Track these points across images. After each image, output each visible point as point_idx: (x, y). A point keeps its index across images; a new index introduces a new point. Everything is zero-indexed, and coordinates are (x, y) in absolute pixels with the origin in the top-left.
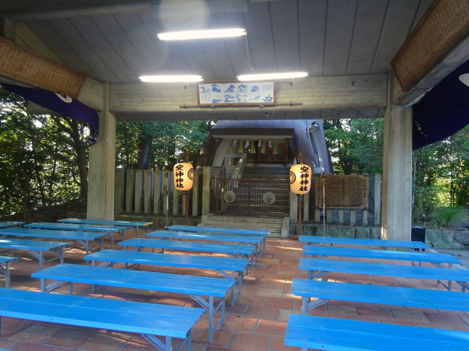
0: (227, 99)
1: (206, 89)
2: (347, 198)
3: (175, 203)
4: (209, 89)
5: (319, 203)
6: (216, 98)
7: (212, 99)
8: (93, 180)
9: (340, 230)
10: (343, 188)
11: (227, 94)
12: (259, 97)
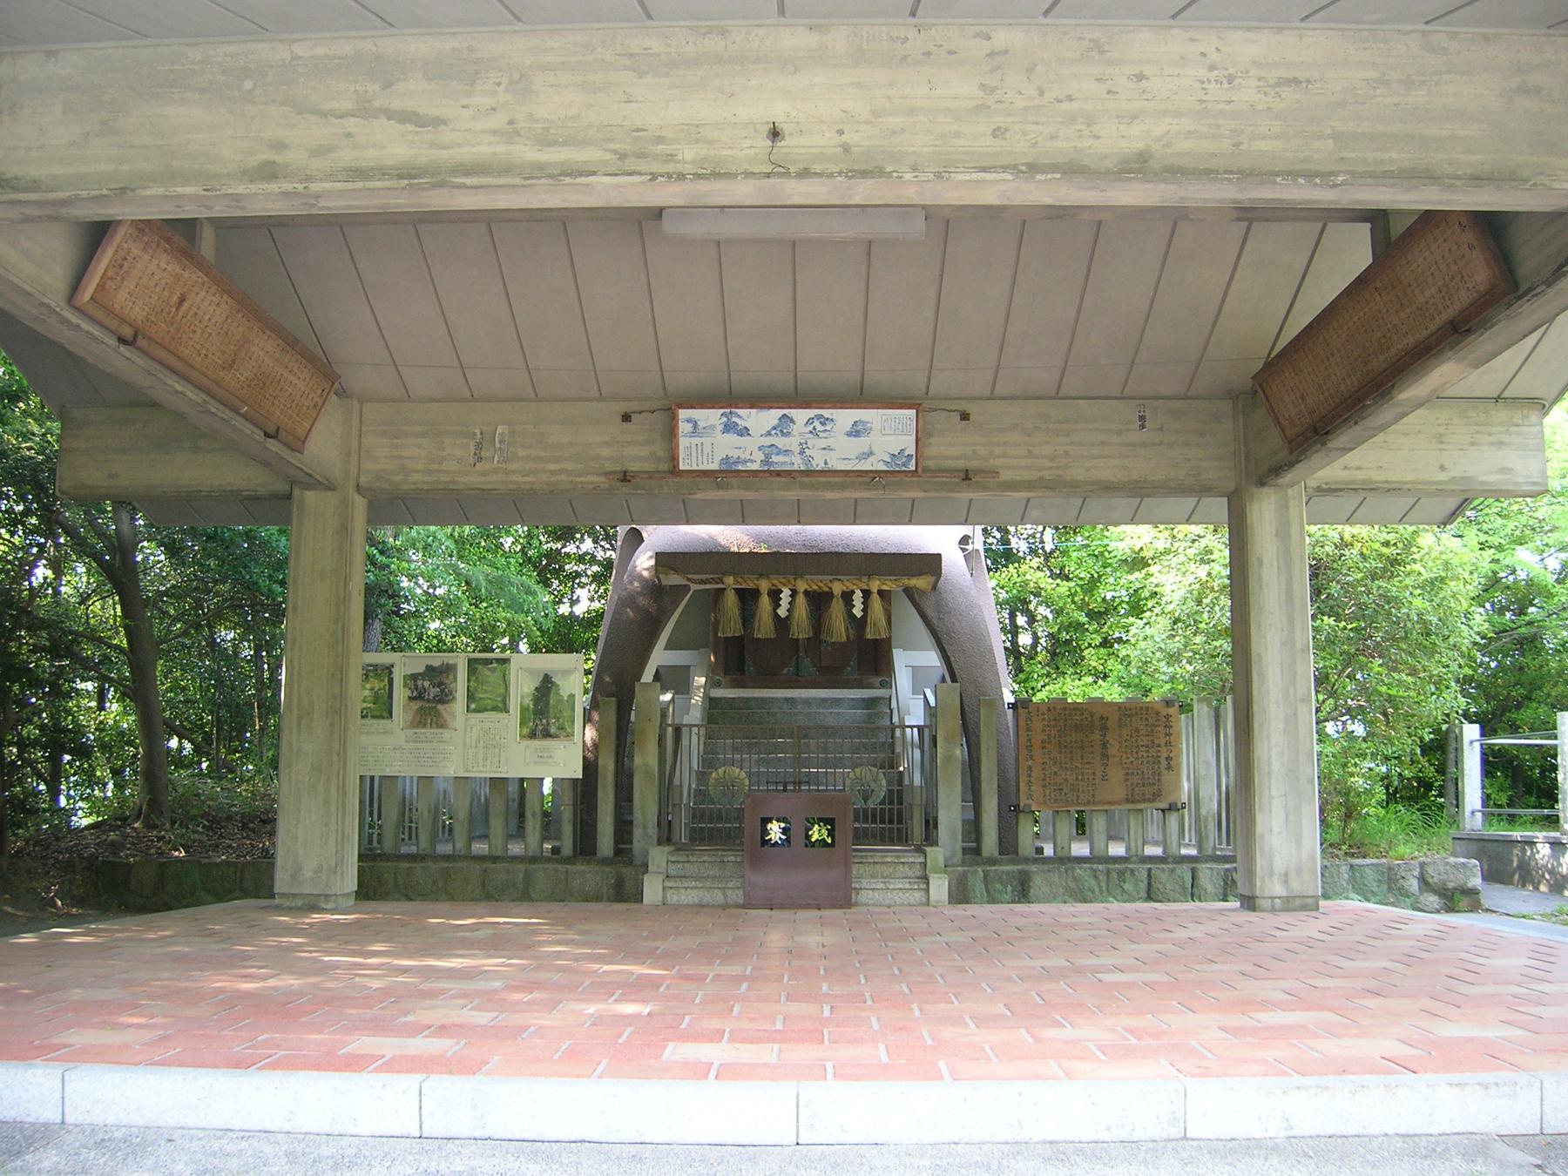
0: (768, 456)
1: (701, 424)
2: (1116, 774)
3: (534, 815)
4: (713, 427)
5: (1030, 796)
6: (735, 454)
7: (718, 458)
8: (299, 724)
9: (1102, 878)
10: (1104, 745)
11: (768, 441)
12: (871, 453)
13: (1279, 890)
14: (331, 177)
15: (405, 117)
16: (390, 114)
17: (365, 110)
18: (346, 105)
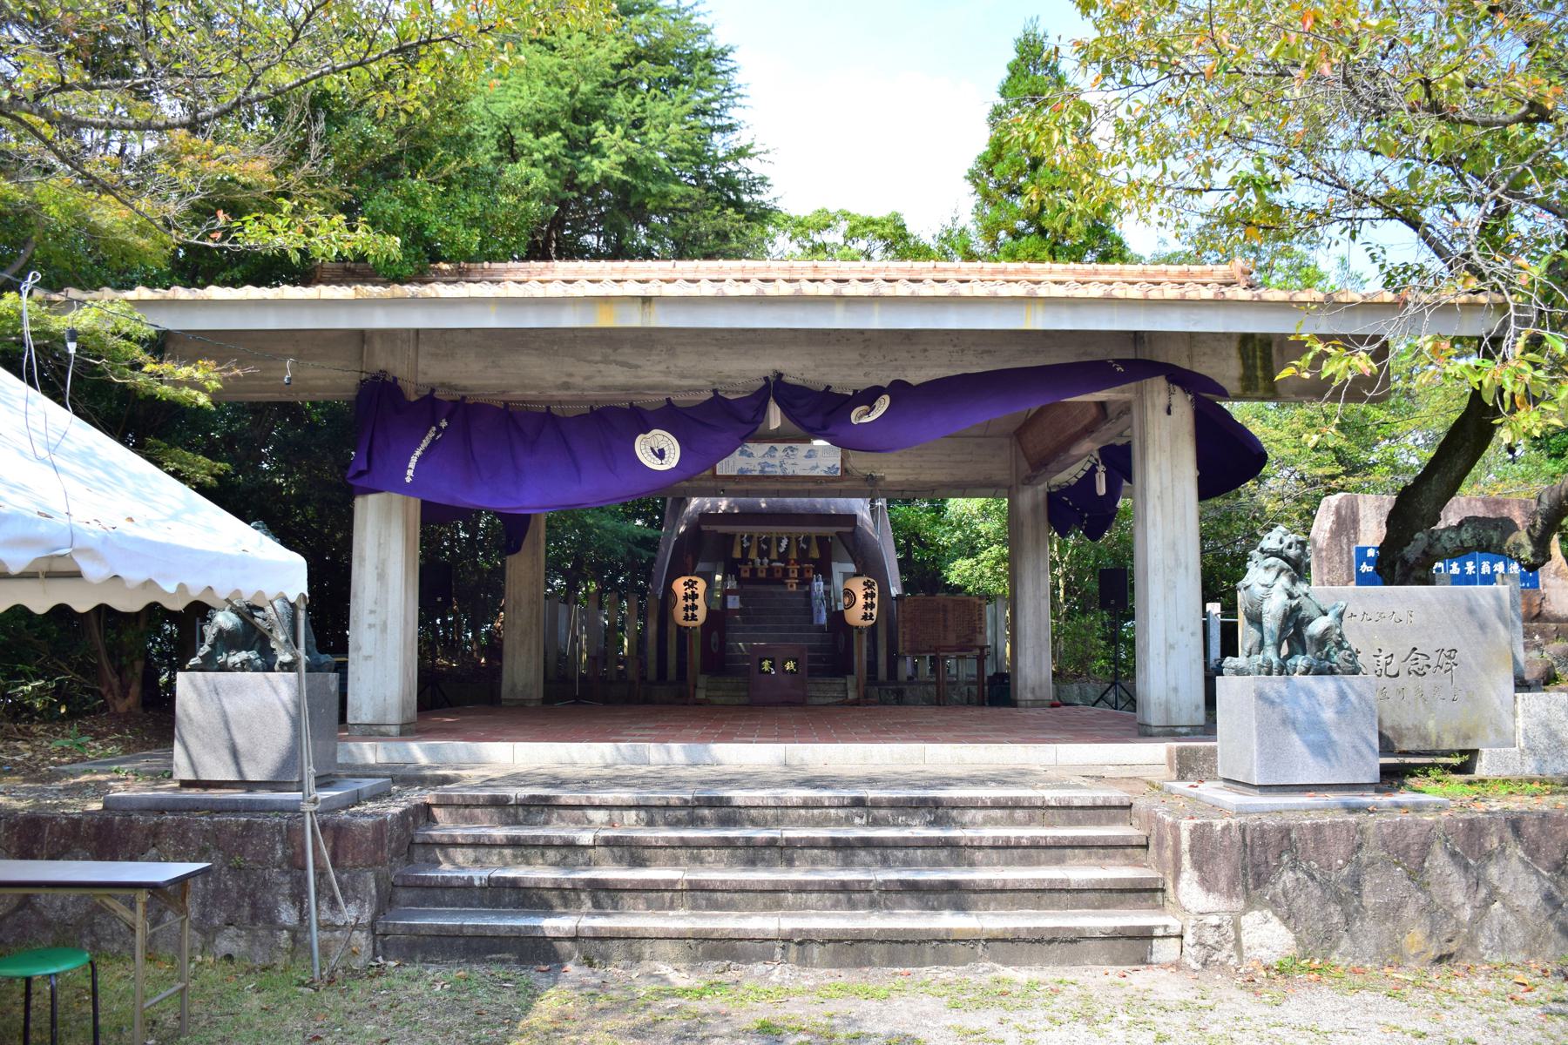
13: (1029, 696)
14: (592, 389)
15: (623, 364)
16: (617, 363)
17: (606, 361)
18: (598, 358)
